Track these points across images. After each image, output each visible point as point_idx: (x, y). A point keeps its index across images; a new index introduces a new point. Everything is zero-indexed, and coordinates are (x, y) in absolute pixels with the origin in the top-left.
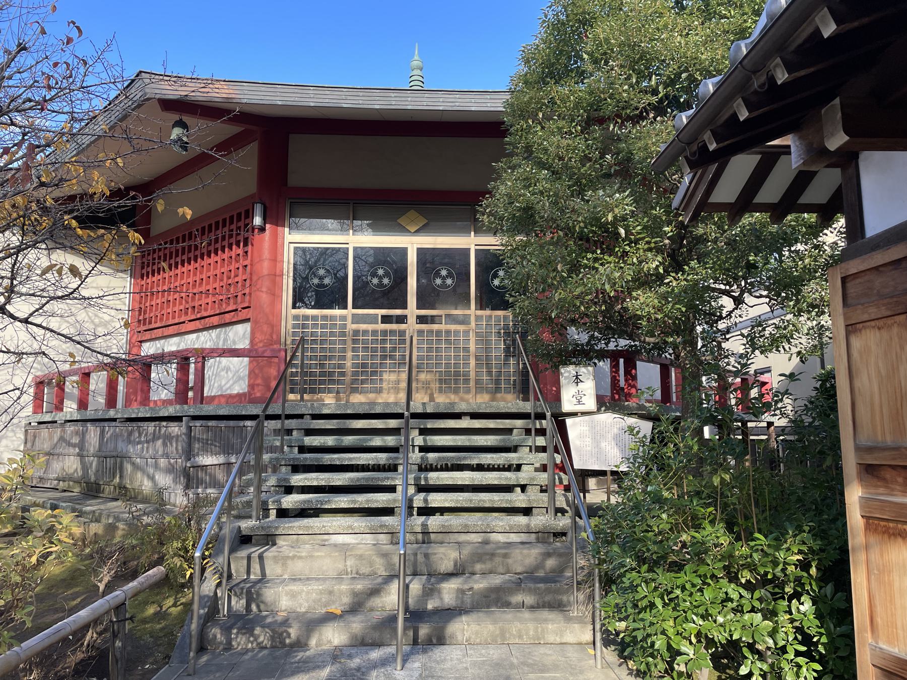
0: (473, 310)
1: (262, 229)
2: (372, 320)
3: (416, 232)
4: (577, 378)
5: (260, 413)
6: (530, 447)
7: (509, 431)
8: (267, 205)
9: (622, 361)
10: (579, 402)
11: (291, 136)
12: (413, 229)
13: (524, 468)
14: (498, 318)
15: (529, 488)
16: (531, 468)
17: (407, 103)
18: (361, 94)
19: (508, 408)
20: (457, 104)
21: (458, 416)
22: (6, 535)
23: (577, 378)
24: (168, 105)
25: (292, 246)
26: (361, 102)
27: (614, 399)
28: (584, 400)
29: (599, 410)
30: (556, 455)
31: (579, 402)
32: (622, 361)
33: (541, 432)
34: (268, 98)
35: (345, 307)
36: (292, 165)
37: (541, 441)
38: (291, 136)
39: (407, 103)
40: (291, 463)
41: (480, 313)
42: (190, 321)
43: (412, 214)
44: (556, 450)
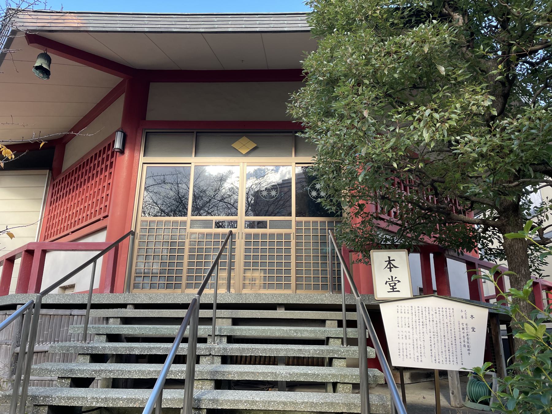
0: (293, 218)
1: (122, 152)
2: (207, 224)
3: (248, 154)
4: (390, 263)
5: (86, 302)
6: (342, 339)
7: (322, 322)
8: (128, 134)
9: (431, 255)
10: (393, 289)
11: (152, 84)
12: (244, 152)
13: (335, 362)
14: (315, 223)
15: (340, 387)
16: (343, 363)
17: (228, 26)
18: (188, 20)
19: (322, 300)
20: (272, 26)
21: (272, 307)
22: (549, 321)
23: (390, 263)
24: (35, 38)
25: (145, 165)
26: (188, 26)
27: (434, 284)
28: (398, 287)
29: (420, 295)
30: (369, 349)
31: (393, 289)
32: (431, 255)
33: (352, 324)
34: (109, 25)
35: (185, 214)
36: (151, 105)
37: (352, 333)
38: (152, 84)
39: (228, 26)
40: (90, 352)
41: (299, 219)
42: (72, 232)
43: (244, 140)
44: (369, 343)
